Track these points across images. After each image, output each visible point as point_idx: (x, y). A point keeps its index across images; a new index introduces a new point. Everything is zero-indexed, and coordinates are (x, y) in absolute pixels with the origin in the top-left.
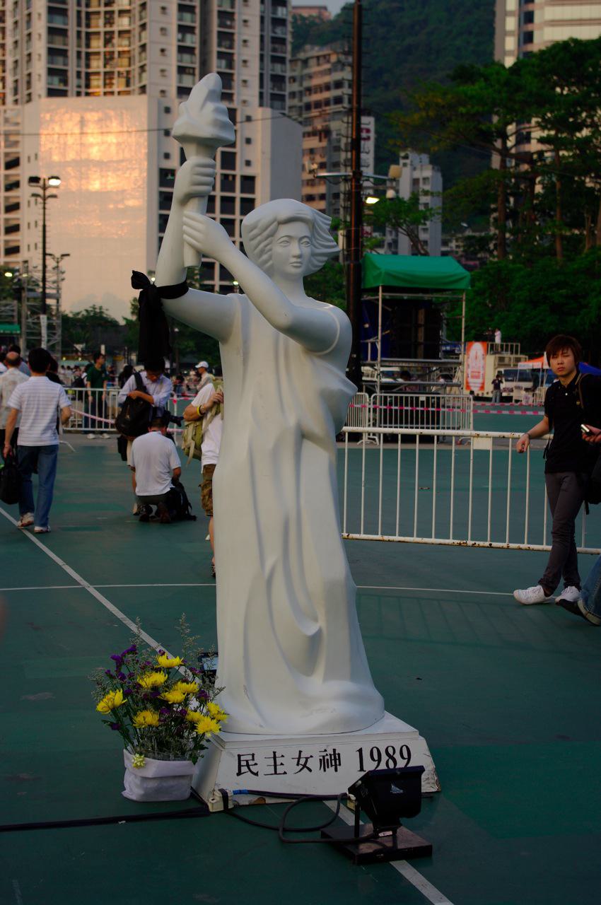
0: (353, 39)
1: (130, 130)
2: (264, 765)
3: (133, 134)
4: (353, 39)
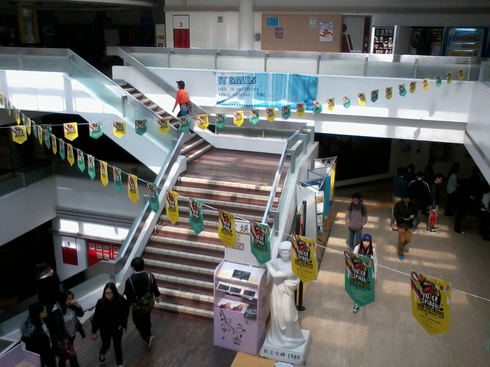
0: (61, 150)
1: (361, 219)
2: (269, 352)
3: (363, 219)
4: (61, 150)
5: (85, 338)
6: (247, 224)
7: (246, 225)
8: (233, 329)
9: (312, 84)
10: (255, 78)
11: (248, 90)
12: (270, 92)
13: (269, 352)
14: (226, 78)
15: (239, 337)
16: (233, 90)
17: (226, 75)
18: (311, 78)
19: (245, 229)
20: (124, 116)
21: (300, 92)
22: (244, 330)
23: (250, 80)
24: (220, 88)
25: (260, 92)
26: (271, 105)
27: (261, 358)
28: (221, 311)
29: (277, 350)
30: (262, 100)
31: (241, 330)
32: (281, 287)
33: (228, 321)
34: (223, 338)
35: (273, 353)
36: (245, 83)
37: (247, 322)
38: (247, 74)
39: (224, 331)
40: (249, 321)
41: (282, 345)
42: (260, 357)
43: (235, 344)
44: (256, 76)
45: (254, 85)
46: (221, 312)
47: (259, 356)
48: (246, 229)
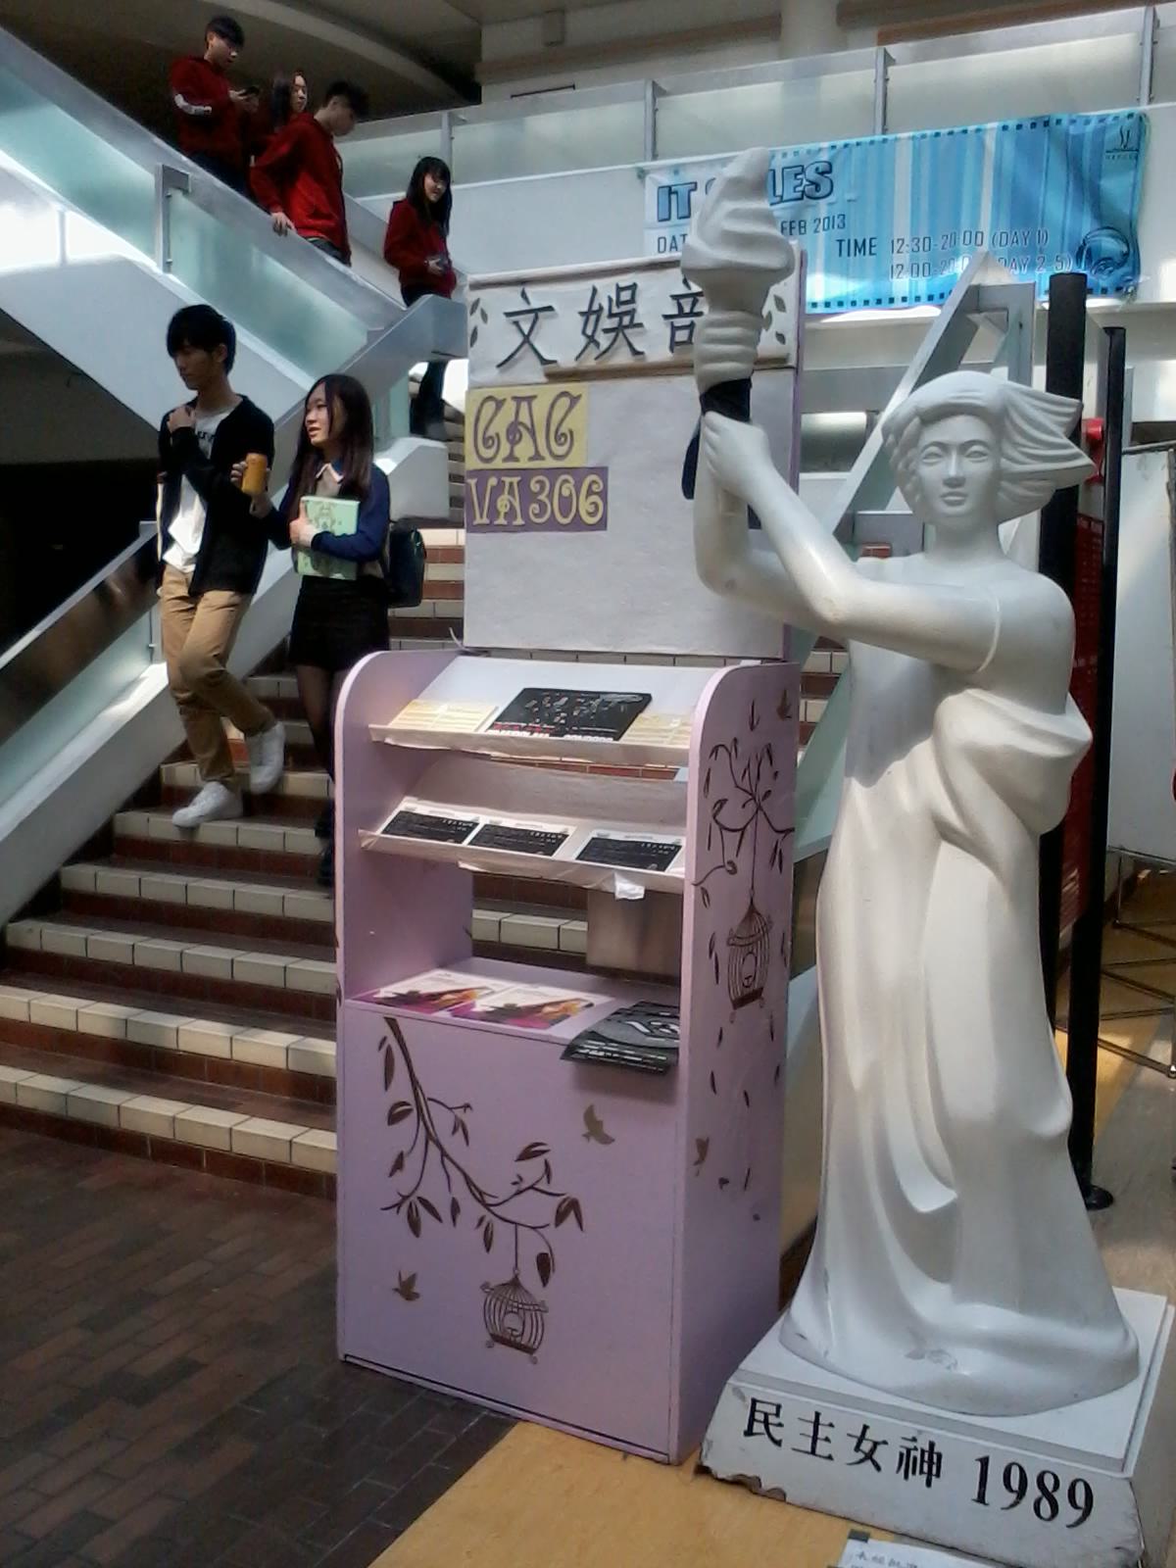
6: (625, 280)
7: (619, 289)
8: (479, 1196)
9: (1116, 150)
10: (830, 171)
11: (795, 231)
12: (902, 227)
13: (794, 1430)
14: (695, 189)
15: (530, 1277)
17: (689, 176)
18: (1110, 120)
19: (613, 323)
20: (168, 266)
21: (1059, 209)
22: (569, 1209)
23: (805, 182)
24: (662, 241)
25: (855, 234)
26: (907, 294)
27: (717, 1484)
28: (387, 1031)
29: (869, 1418)
30: (859, 275)
31: (547, 1208)
32: (913, 780)
33: (442, 1121)
34: (407, 1290)
35: (822, 1448)
36: (782, 197)
37: (594, 1128)
38: (790, 156)
39: (415, 1226)
40: (610, 1108)
41: (924, 1372)
42: (703, 1482)
44: (834, 157)
45: (822, 203)
46: (392, 1041)
47: (703, 1471)
48: (618, 330)
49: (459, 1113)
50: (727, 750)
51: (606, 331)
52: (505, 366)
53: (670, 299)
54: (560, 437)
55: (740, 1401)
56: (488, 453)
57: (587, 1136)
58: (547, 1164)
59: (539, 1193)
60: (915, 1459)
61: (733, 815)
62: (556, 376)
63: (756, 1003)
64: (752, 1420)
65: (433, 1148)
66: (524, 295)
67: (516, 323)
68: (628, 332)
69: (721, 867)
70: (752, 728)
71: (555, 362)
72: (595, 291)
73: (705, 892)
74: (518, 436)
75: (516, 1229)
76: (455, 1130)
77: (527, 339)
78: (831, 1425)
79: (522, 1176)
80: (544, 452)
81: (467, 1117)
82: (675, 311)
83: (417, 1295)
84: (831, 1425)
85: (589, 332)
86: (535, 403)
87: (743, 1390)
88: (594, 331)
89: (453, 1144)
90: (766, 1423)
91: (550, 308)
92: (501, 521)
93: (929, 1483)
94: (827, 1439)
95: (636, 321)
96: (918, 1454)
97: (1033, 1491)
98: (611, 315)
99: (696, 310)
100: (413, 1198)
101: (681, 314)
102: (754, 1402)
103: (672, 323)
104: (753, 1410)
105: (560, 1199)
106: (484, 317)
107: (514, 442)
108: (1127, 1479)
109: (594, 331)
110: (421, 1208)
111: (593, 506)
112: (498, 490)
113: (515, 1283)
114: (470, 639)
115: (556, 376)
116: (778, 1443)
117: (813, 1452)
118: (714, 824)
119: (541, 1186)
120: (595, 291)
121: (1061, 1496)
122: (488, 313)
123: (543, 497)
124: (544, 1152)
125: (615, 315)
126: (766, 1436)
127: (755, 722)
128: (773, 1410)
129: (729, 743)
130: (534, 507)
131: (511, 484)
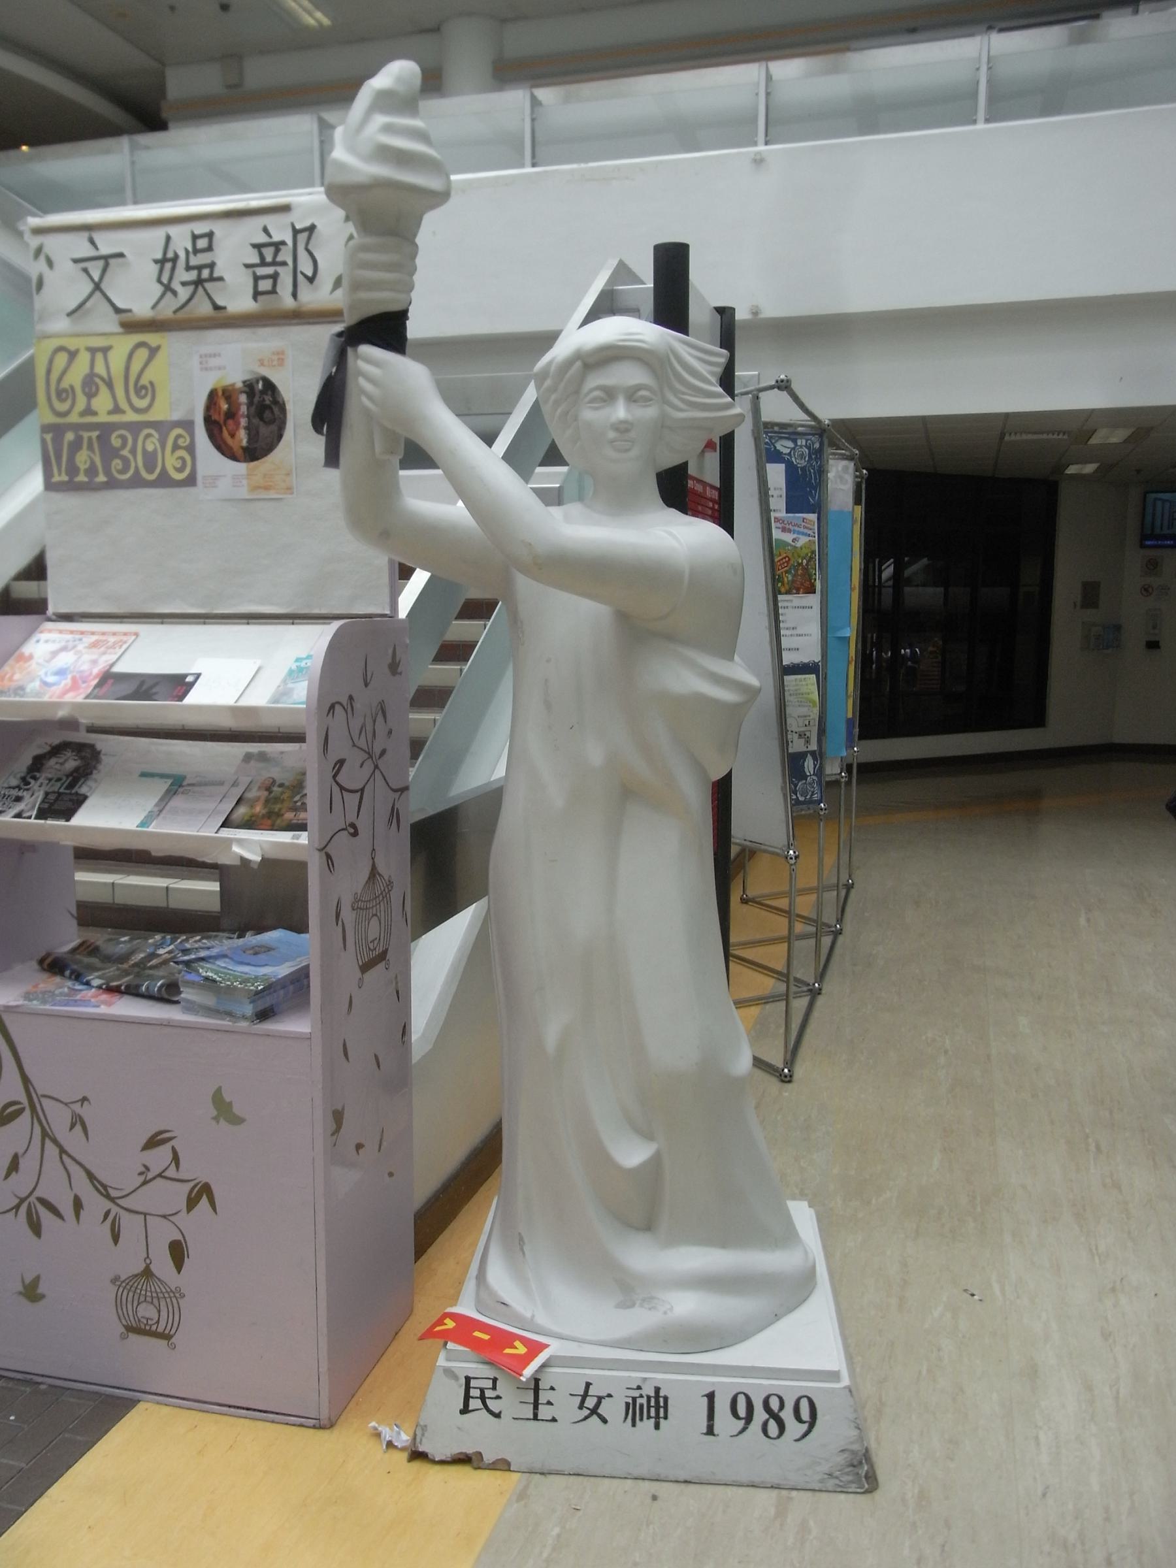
5: (590, 1381)
6: (201, 228)
7: (195, 237)
8: (103, 1190)
15: (163, 1266)
16: (265, 476)
19: (192, 276)
22: (201, 1193)
31: (175, 1195)
33: (58, 1118)
34: (31, 1292)
35: (544, 1412)
39: (36, 1228)
43: (133, 1337)
48: (198, 282)
49: (77, 1107)
50: (344, 708)
51: (184, 284)
52: (76, 315)
53: (250, 247)
54: (140, 390)
55: (453, 1381)
56: (62, 407)
57: (216, 1119)
58: (174, 1150)
59: (169, 1182)
60: (641, 1406)
61: (352, 776)
62: (132, 326)
63: (381, 966)
64: (467, 1397)
65: (49, 1144)
66: (92, 242)
67: (85, 270)
68: (208, 285)
69: (343, 829)
70: (366, 685)
71: (129, 311)
72: (168, 238)
73: (328, 857)
74: (94, 389)
75: (145, 1220)
76: (72, 1126)
77: (97, 287)
78: (552, 1388)
79: (148, 1164)
80: (123, 404)
81: (84, 1111)
82: (256, 260)
83: (43, 1296)
84: (552, 1388)
85: (165, 280)
86: (111, 355)
87: (453, 1369)
88: (171, 279)
89: (72, 1140)
90: (483, 1398)
91: (121, 255)
92: (82, 478)
93: (657, 1426)
94: (549, 1403)
95: (216, 275)
96: (644, 1401)
97: (760, 1415)
98: (189, 268)
99: (279, 259)
100: (32, 1199)
101: (263, 263)
102: (468, 1379)
103: (254, 274)
104: (468, 1388)
105: (192, 1184)
106: (50, 263)
107: (90, 395)
108: (845, 1388)
109: (171, 279)
110: (39, 1207)
111: (180, 461)
112: (76, 446)
113: (147, 1273)
114: (51, 610)
115: (132, 326)
116: (497, 1416)
117: (535, 1418)
118: (334, 783)
119: (171, 1172)
120: (168, 238)
121: (787, 1415)
122: (53, 258)
123: (125, 452)
124: (170, 1139)
125: (193, 268)
126: (485, 1411)
127: (369, 677)
128: (489, 1384)
129: (344, 701)
130: (117, 464)
131: (90, 439)
